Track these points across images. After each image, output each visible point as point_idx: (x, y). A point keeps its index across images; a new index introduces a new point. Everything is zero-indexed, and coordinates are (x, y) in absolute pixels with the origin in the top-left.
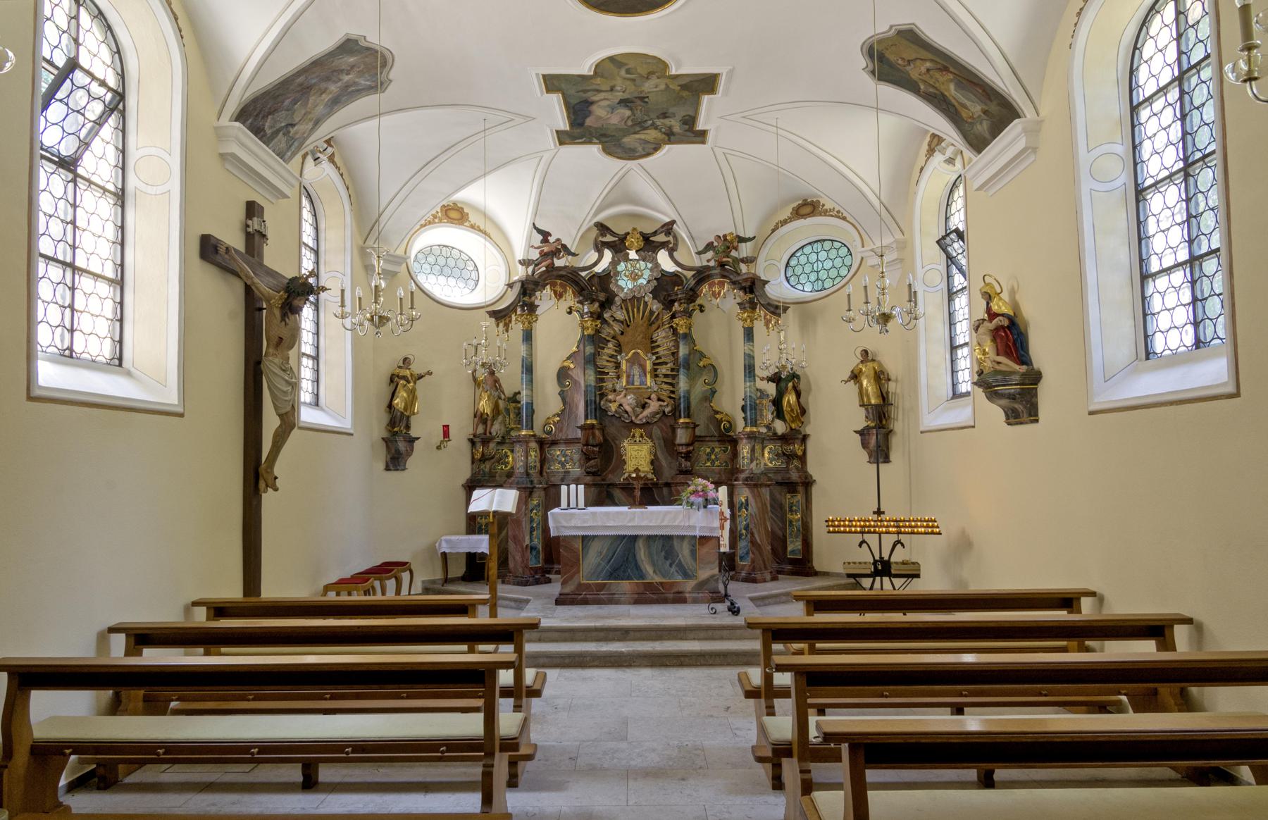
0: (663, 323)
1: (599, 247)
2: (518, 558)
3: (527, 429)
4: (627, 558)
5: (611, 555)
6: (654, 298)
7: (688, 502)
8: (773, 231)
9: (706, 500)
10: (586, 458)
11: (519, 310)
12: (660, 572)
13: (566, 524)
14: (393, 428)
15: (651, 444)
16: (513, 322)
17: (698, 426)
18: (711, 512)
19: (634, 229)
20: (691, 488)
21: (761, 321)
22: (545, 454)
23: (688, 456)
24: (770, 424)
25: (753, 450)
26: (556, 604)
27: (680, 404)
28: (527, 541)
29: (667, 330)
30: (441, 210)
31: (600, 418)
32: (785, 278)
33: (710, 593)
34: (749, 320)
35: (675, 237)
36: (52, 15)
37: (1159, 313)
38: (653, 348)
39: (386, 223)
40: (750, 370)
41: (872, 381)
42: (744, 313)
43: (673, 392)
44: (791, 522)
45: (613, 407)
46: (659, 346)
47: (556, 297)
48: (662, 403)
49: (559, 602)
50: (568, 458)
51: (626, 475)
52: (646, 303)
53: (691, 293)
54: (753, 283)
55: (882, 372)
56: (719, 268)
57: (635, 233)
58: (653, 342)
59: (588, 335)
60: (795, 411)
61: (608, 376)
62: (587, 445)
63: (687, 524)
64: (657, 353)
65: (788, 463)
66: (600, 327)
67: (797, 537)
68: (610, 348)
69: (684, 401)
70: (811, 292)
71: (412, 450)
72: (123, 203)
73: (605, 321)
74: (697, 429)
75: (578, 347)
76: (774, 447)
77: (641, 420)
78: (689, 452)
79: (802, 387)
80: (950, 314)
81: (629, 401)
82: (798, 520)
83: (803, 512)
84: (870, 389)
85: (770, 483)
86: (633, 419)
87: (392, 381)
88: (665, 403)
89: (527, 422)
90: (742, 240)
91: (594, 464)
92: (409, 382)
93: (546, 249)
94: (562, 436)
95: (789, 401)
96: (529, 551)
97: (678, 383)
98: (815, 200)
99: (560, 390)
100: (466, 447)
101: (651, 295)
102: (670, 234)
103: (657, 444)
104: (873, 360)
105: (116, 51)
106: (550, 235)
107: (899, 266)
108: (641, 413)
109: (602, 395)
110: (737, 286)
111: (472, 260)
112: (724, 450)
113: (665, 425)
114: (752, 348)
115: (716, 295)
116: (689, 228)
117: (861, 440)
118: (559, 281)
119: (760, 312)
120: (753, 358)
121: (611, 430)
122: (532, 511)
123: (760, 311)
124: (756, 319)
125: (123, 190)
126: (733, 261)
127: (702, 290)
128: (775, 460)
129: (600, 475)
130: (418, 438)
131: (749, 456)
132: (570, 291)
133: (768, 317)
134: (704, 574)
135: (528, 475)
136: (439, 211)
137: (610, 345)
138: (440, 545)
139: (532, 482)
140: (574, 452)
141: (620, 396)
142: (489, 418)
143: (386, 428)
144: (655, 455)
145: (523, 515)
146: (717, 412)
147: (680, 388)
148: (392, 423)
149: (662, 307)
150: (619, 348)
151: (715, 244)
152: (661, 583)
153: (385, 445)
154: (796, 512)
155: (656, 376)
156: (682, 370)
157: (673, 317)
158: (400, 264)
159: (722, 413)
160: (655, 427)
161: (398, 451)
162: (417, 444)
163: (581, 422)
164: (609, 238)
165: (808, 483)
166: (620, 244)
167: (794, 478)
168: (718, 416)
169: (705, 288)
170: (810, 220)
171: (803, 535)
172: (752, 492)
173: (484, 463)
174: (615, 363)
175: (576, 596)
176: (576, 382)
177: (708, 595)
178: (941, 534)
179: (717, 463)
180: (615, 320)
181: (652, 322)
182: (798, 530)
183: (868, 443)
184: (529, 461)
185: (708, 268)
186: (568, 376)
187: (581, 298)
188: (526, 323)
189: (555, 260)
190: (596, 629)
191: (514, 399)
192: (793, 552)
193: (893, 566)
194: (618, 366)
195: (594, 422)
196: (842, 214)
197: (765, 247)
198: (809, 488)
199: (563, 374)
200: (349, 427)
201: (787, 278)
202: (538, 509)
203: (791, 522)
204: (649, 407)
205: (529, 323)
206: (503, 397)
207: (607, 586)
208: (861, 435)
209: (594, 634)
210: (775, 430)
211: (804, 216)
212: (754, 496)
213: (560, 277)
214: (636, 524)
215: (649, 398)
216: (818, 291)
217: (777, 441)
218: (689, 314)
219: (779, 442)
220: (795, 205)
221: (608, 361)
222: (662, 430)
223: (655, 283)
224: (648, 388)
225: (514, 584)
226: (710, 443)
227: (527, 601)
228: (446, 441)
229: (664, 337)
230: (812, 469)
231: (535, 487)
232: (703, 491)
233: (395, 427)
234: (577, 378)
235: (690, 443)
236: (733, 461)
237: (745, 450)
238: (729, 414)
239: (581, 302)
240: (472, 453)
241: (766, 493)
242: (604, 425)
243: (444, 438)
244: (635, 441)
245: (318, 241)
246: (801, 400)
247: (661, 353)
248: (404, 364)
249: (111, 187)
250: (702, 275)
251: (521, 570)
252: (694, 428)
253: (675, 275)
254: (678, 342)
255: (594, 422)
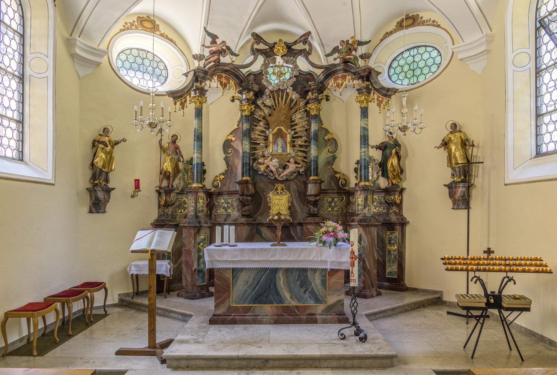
0: (300, 108)
1: (255, 52)
2: (189, 279)
3: (197, 182)
4: (269, 286)
5: (256, 283)
6: (293, 90)
7: (320, 241)
8: (381, 40)
9: (337, 239)
10: (242, 205)
11: (193, 93)
12: (296, 297)
13: (219, 259)
14: (94, 181)
15: (289, 195)
16: (188, 102)
17: (323, 182)
18: (340, 249)
19: (280, 40)
20: (324, 229)
21: (374, 102)
22: (214, 202)
23: (315, 204)
24: (375, 181)
25: (366, 199)
26: (210, 324)
27: (311, 166)
28: (195, 266)
29: (302, 113)
30: (137, 20)
31: (253, 176)
32: (388, 76)
33: (337, 315)
34: (365, 102)
35: (310, 45)
36: (11, 4)
37: (544, 134)
38: (292, 126)
39: (87, 22)
40: (365, 139)
41: (459, 147)
42: (362, 96)
43: (305, 158)
44: (389, 251)
45: (262, 168)
46: (296, 125)
47: (222, 86)
48: (298, 165)
49: (214, 321)
50: (229, 205)
51: (271, 217)
52: (288, 93)
53: (321, 85)
54: (370, 73)
55: (467, 140)
56: (343, 64)
57: (281, 43)
58: (292, 122)
59: (246, 116)
60: (396, 170)
61: (259, 146)
62: (243, 195)
63: (319, 259)
64: (295, 129)
65: (388, 209)
66: (254, 111)
67: (393, 262)
68: (261, 126)
69: (314, 164)
70: (408, 85)
71: (109, 198)
72: (23, 82)
73: (257, 106)
74: (323, 185)
75: (238, 125)
76: (378, 197)
77: (282, 177)
78: (317, 201)
79: (402, 153)
80: (536, 88)
81: (274, 164)
82: (395, 250)
83: (399, 244)
84: (457, 154)
85: (378, 223)
86: (277, 176)
87: (94, 145)
88: (300, 166)
89: (197, 177)
90: (360, 43)
91: (248, 209)
92: (107, 147)
93: (214, 49)
94: (225, 189)
95: (392, 163)
96: (197, 273)
97: (310, 151)
98: (415, 14)
99: (225, 156)
100: (155, 196)
101: (291, 88)
102: (306, 42)
103: (293, 195)
104: (460, 131)
105: (19, 4)
106: (218, 38)
107: (486, 57)
108: (283, 172)
109: (255, 160)
110: (356, 76)
111: (162, 62)
112: (340, 200)
113: (300, 181)
114: (366, 123)
115: (339, 86)
116: (321, 36)
117: (449, 193)
118: (224, 75)
119: (375, 96)
120: (368, 130)
121: (261, 185)
122: (199, 244)
123: (374, 95)
124: (371, 101)
125: (23, 75)
126: (354, 58)
127: (329, 83)
128: (378, 206)
129: (252, 217)
130: (113, 189)
131: (363, 203)
132: (232, 82)
133: (380, 99)
134: (332, 300)
135: (197, 217)
136: (136, 20)
137: (261, 124)
138: (130, 268)
139: (199, 222)
140: (234, 201)
141: (268, 160)
142: (171, 175)
143: (89, 181)
144: (292, 203)
145: (193, 247)
146: (336, 173)
147: (311, 154)
148: (94, 177)
149: (299, 96)
150: (268, 126)
151: (340, 47)
152: (297, 307)
153: (89, 193)
154: (394, 244)
155: (294, 146)
156: (312, 141)
157: (307, 103)
158: (102, 56)
159: (340, 173)
160: (292, 183)
161: (97, 199)
162: (112, 193)
163: (239, 178)
164: (262, 46)
165: (403, 224)
166: (270, 52)
167: (393, 220)
168: (337, 175)
169: (331, 82)
170: (411, 30)
171: (399, 261)
172: (365, 231)
173: (167, 208)
174: (264, 136)
175: (226, 317)
176: (236, 151)
177: (335, 317)
178: (552, 273)
179: (336, 209)
180: (265, 106)
181: (292, 106)
182: (395, 257)
183: (455, 194)
184: (198, 207)
185: (334, 65)
186: (231, 147)
187: (241, 89)
188: (198, 103)
189: (221, 58)
190: (239, 358)
191: (190, 162)
192: (390, 273)
193: (504, 299)
194: (266, 139)
195: (248, 178)
196: (437, 23)
197: (375, 52)
198: (404, 227)
199: (227, 145)
200: (51, 178)
201: (389, 76)
202: (205, 242)
203: (389, 251)
204: (288, 168)
205: (200, 103)
206: (182, 160)
207: (252, 310)
208: (449, 188)
209: (237, 362)
210: (379, 185)
211: (407, 27)
212: (366, 234)
213: (226, 71)
214: (277, 259)
215: (289, 162)
216: (413, 84)
217: (380, 193)
218: (319, 101)
219: (384, 193)
220: (399, 19)
221: (259, 135)
222: (296, 184)
223: (295, 79)
224: (288, 154)
225: (185, 298)
226: (330, 195)
227: (191, 316)
228: (137, 192)
229: (300, 118)
230: (405, 214)
231: (201, 226)
232: (333, 231)
233: (96, 180)
234: (237, 148)
235: (318, 194)
236: (347, 207)
237: (359, 199)
238: (345, 174)
239: (240, 92)
240: (159, 201)
241: (374, 231)
242: (255, 181)
243: (135, 189)
244: (278, 193)
245: (23, 26)
246: (400, 163)
247: (298, 130)
248: (103, 132)
249: (16, 73)
250: (330, 72)
251: (190, 287)
252: (320, 183)
253: (310, 74)
254: (311, 122)
255: (248, 178)
